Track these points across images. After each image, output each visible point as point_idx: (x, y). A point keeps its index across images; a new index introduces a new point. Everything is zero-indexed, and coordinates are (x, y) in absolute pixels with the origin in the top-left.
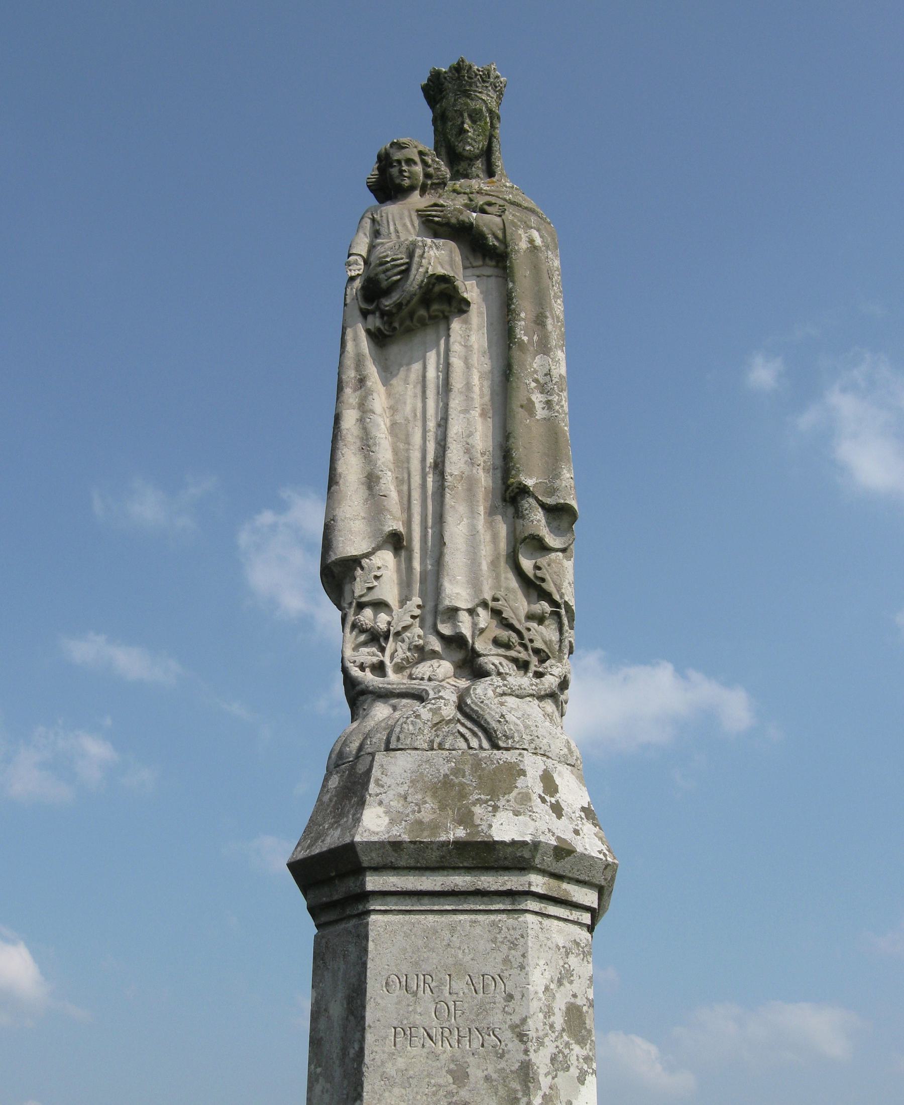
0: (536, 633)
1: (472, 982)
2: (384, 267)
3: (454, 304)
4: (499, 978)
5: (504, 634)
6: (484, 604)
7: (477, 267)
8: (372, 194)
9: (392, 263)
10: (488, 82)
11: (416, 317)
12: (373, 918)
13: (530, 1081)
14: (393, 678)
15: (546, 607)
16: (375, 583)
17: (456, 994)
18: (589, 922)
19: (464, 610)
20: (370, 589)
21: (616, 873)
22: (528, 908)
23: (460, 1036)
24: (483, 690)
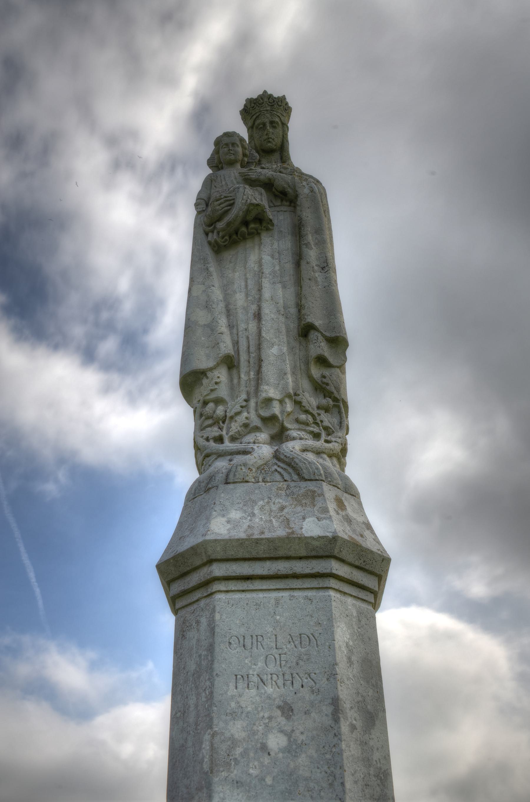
0: (324, 417)
1: (292, 639)
2: (219, 202)
3: (264, 224)
4: (312, 637)
5: (303, 417)
6: (289, 396)
7: (278, 206)
9: (224, 199)
10: (281, 106)
11: (239, 233)
12: (218, 596)
13: (340, 713)
14: (228, 445)
16: (216, 387)
17: (281, 649)
18: (373, 601)
19: (276, 400)
20: (212, 390)
22: (331, 586)
23: (286, 680)
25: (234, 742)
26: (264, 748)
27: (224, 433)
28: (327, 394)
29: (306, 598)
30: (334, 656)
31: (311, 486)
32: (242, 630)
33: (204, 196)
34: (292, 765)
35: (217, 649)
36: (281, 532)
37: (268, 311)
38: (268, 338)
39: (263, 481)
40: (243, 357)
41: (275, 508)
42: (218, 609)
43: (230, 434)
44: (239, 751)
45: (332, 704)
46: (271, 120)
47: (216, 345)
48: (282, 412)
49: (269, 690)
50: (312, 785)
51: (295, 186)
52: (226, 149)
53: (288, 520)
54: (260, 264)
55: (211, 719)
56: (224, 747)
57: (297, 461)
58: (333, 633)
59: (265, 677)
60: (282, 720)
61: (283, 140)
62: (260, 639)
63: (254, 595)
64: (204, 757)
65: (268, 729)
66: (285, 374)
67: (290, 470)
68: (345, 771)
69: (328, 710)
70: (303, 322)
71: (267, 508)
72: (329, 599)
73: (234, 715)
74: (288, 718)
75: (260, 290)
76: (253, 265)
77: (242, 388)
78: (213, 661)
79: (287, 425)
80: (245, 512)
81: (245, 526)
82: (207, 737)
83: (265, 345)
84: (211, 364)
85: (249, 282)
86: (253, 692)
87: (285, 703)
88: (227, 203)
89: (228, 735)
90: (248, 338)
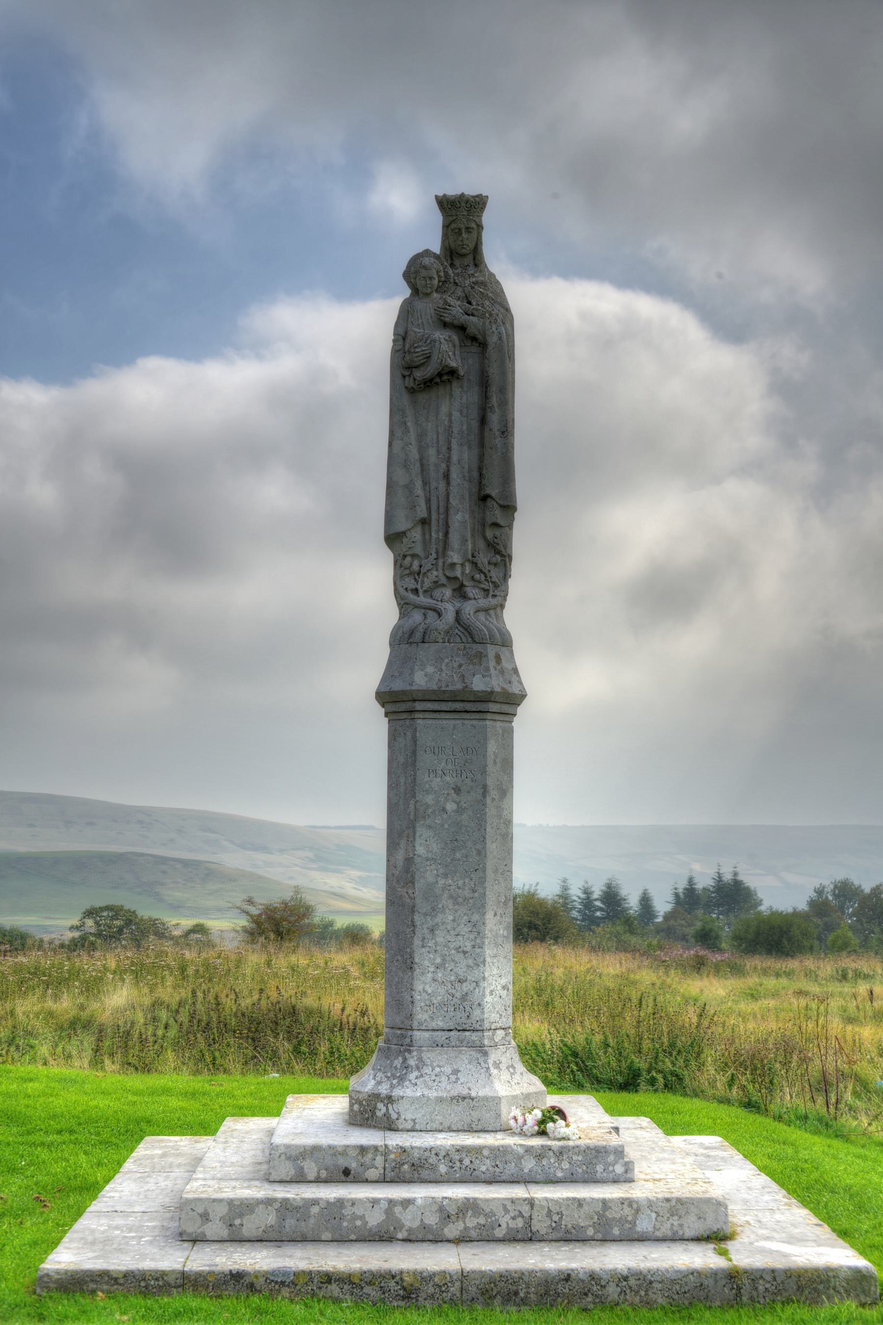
8: (389, 650)
15: (499, 558)
16: (413, 545)
21: (69, 1229)
24: (469, 608)
25: (428, 806)
26: (444, 810)
27: (419, 587)
28: (498, 552)
29: (472, 725)
30: (486, 761)
31: (479, 647)
32: (433, 743)
33: (401, 331)
34: (459, 819)
35: (418, 754)
36: (459, 686)
37: (454, 475)
38: (454, 504)
39: (448, 642)
40: (434, 516)
41: (456, 665)
42: (418, 729)
43: (424, 589)
44: (430, 810)
45: (483, 788)
46: (467, 226)
47: (413, 507)
48: (463, 573)
49: (448, 779)
50: (469, 829)
51: (485, 333)
52: (423, 282)
53: (463, 676)
54: (450, 415)
55: (415, 793)
56: (422, 808)
57: (472, 629)
58: (486, 748)
59: (445, 772)
60: (454, 796)
61: (477, 242)
62: (443, 749)
63: (440, 722)
64: (410, 812)
65: (446, 800)
66: (466, 541)
67: (467, 634)
68: (484, 980)
69: (481, 791)
70: (483, 493)
71: (450, 664)
72: (485, 727)
73: (427, 792)
74: (458, 794)
75: (449, 449)
76: (444, 418)
77: (432, 546)
78: (415, 761)
79: (465, 583)
80: (436, 667)
81: (436, 680)
82: (412, 802)
83: (451, 512)
84: (409, 525)
85: (440, 437)
86: (439, 779)
87: (457, 786)
88: (425, 356)
89: (424, 802)
90: (438, 497)
